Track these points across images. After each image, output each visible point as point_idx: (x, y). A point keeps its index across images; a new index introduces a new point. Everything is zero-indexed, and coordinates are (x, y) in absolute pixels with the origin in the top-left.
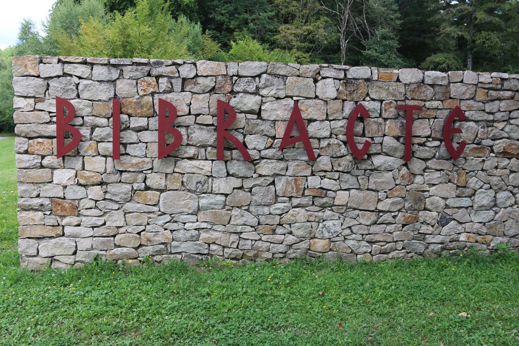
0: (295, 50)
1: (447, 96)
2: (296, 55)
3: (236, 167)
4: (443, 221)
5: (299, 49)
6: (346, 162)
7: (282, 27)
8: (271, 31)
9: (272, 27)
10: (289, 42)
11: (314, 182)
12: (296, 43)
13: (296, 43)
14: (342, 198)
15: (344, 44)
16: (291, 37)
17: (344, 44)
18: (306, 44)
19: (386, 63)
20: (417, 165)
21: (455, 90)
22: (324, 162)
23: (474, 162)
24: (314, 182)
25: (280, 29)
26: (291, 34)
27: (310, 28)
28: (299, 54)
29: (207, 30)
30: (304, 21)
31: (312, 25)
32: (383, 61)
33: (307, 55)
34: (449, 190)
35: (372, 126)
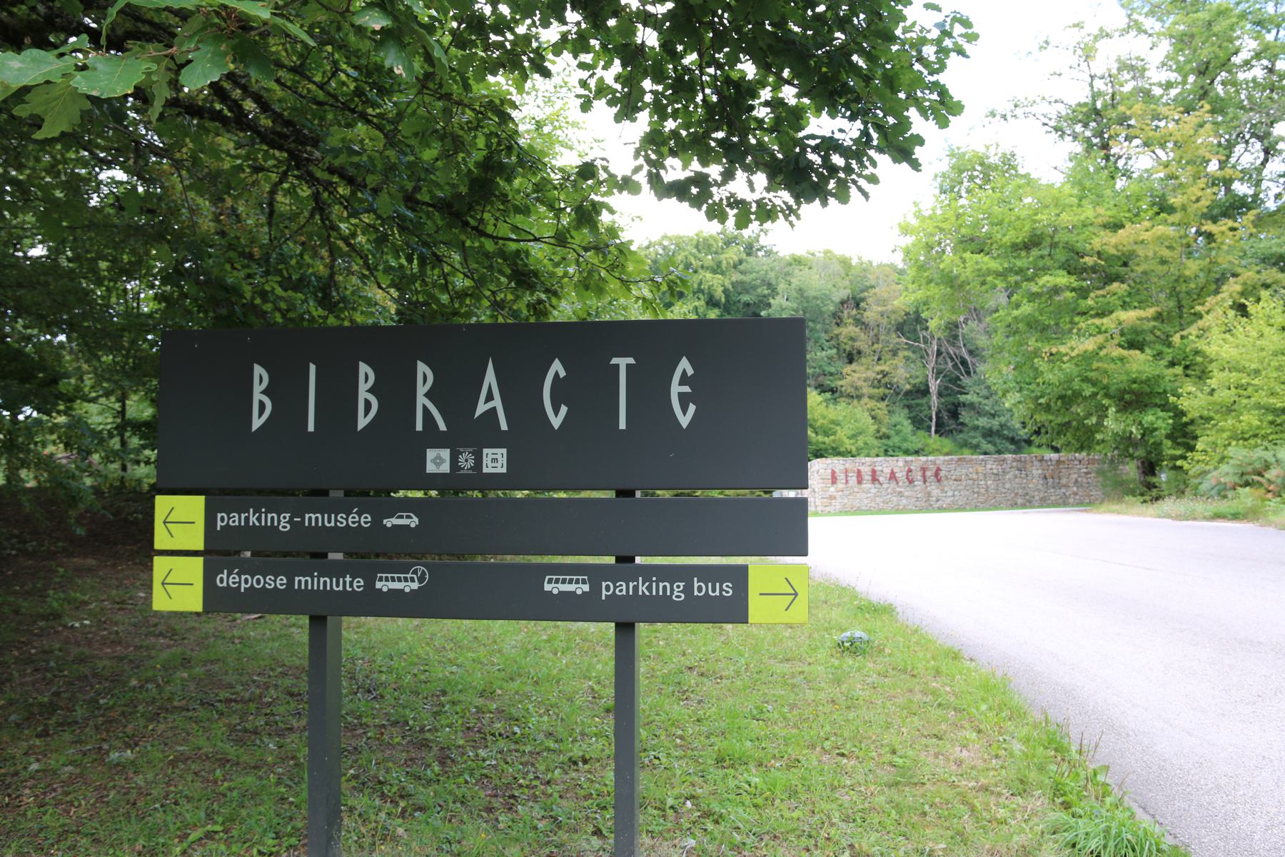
0: (865, 400)
1: (935, 464)
2: (869, 406)
3: (877, 486)
4: (938, 500)
5: (871, 397)
6: (907, 483)
7: (848, 369)
8: (831, 374)
9: (833, 370)
10: (856, 389)
11: (898, 489)
12: (866, 390)
13: (866, 390)
14: (906, 494)
15: (934, 386)
16: (859, 383)
17: (934, 386)
18: (882, 390)
19: (993, 412)
20: (928, 484)
21: (938, 462)
22: (901, 484)
23: (945, 483)
24: (898, 489)
25: (844, 371)
26: (859, 379)
27: (886, 368)
28: (872, 404)
29: (419, 197)
30: (876, 358)
31: (888, 363)
32: (987, 408)
33: (882, 405)
34: (938, 491)
35: (914, 473)
